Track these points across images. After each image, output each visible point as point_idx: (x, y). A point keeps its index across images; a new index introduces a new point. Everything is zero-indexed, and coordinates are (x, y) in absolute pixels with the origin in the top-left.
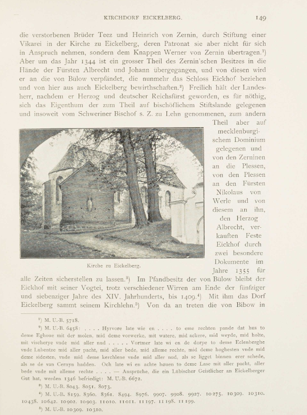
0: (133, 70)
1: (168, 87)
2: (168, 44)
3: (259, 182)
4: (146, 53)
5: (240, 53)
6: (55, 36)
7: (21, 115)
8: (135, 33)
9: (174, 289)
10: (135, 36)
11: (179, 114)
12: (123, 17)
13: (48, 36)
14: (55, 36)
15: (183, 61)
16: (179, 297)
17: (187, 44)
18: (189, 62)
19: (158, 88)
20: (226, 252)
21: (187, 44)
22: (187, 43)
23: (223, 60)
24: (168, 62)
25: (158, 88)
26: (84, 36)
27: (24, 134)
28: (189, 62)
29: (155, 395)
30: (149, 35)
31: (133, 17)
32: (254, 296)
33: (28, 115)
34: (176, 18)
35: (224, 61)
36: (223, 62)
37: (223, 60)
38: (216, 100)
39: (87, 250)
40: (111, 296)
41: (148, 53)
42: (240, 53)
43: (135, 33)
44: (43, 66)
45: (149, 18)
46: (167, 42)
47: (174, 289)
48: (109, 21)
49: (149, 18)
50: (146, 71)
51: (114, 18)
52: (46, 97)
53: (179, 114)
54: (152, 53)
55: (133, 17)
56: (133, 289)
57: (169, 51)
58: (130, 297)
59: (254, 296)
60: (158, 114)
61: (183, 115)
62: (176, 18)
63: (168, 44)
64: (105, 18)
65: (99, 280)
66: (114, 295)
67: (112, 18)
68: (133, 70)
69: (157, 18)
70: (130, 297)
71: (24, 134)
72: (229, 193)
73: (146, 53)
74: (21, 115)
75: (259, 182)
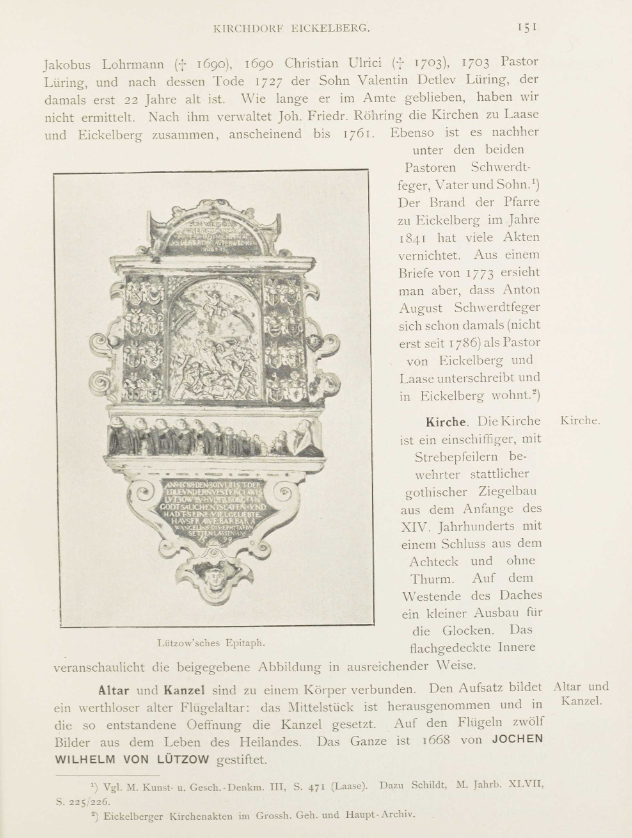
0: (288, 117)
8: (245, 739)
9: (254, 100)
10: (245, 744)
18: (92, 119)
19: (95, 669)
22: (112, 115)
28: (92, 119)
30: (306, 64)
31: (271, 29)
32: (404, 203)
36: (60, 744)
38: (459, 105)
40: (411, 527)
43: (245, 739)
44: (454, 142)
47: (254, 100)
50: (411, 546)
52: (146, 83)
55: (271, 29)
58: (157, 101)
59: (404, 203)
60: (403, 222)
64: (216, 29)
65: (491, 115)
66: (417, 525)
68: (288, 117)
70: (157, 101)
72: (66, 66)
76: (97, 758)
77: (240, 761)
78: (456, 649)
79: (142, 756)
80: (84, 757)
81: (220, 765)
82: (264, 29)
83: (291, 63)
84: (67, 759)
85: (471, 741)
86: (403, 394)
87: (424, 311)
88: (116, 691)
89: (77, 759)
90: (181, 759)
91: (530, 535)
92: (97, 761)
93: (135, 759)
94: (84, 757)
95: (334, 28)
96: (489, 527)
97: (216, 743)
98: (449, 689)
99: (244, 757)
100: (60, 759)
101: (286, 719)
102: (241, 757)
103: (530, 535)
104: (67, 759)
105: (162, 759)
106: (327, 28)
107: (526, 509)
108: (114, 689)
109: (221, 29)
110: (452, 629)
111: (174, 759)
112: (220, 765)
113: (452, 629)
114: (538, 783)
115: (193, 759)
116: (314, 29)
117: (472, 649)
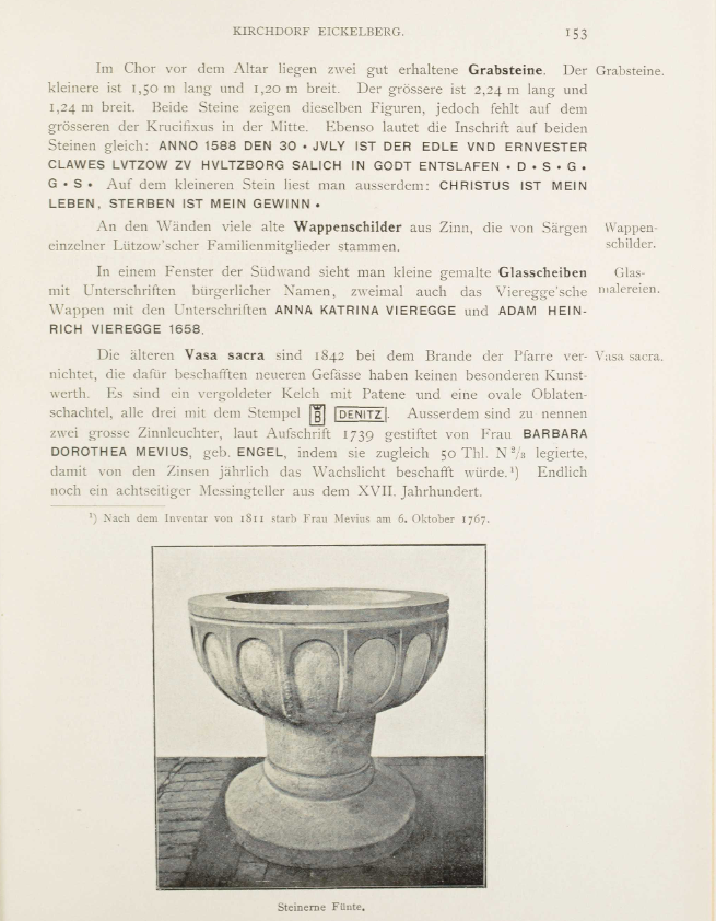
1: (428, 473)
2: (371, 395)
7: (650, 229)
12: (275, 30)
16: (526, 395)
17: (383, 71)
20: (371, 353)
21: (383, 71)
23: (431, 353)
24: (391, 357)
29: (417, 187)
31: (296, 31)
33: (240, 89)
34: (391, 32)
37: (431, 353)
45: (331, 31)
46: (367, 391)
48: (617, 352)
49: (331, 31)
51: (255, 32)
55: (296, 31)
59: (364, 88)
62: (391, 32)
63: (371, 395)
64: (236, 32)
67: (251, 31)
69: (349, 31)
74: (650, 229)
76: (274, 451)
77: (411, 435)
78: (313, 247)
80: (552, 308)
82: (289, 31)
83: (131, 68)
84: (394, 310)
86: (226, 124)
87: (374, 72)
89: (64, 164)
91: (574, 101)
92: (274, 453)
94: (552, 308)
95: (365, 31)
97: (466, 293)
98: (381, 274)
99: (416, 431)
100: (55, 491)
101: (151, 120)
102: (411, 431)
103: (574, 101)
104: (394, 310)
106: (358, 31)
109: (241, 31)
114: (657, 358)
116: (343, 32)
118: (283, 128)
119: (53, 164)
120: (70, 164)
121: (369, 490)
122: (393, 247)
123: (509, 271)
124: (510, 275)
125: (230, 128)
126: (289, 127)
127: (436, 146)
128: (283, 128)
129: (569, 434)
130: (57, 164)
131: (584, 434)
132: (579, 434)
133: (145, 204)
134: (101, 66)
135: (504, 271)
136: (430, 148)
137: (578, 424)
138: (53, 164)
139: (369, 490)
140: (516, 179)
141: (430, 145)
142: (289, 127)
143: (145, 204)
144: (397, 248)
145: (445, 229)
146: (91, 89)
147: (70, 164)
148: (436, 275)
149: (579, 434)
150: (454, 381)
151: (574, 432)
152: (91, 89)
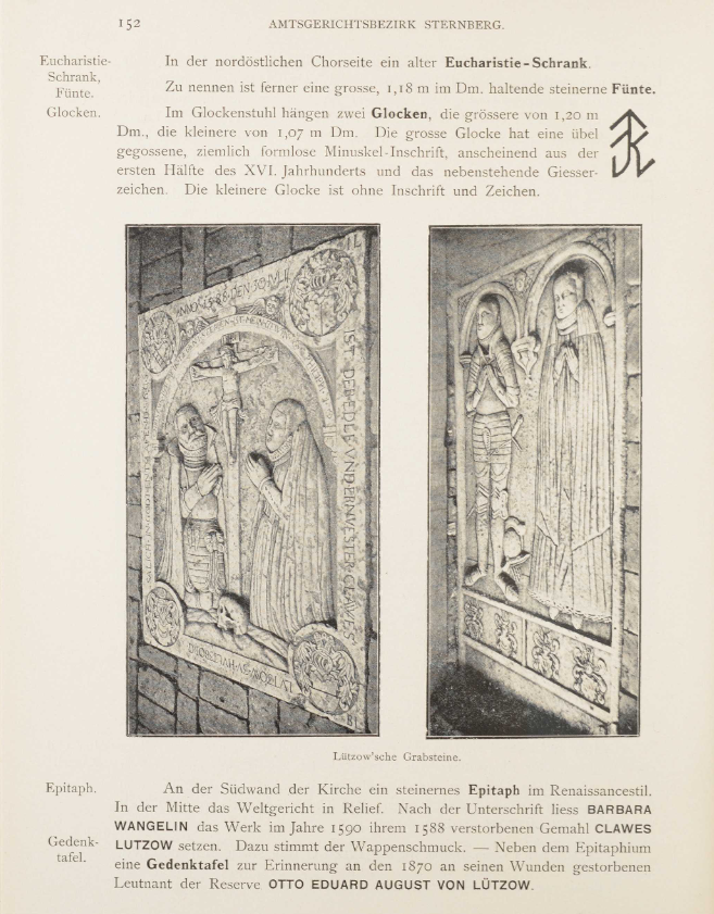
3: (491, 807)
4: (373, 848)
5: (354, 172)
6: (500, 830)
8: (170, 167)
11: (561, 868)
13: (486, 830)
14: (500, 830)
15: (493, 192)
18: (591, 90)
19: (513, 811)
25: (513, 811)
26: (260, 791)
27: (138, 236)
28: (591, 90)
31: (283, 24)
34: (491, 26)
35: (357, 846)
39: (244, 567)
41: (379, 848)
42: (354, 172)
48: (570, 70)
53: (561, 868)
54: (387, 848)
55: (283, 24)
56: (502, 811)
57: (248, 805)
61: (569, 870)
71: (138, 236)
73: (373, 848)
75: (491, 807)
79: (143, 829)
81: (338, 93)
85: (536, 116)
88: (496, 792)
89: (611, 828)
90: (499, 885)
92: (164, 827)
93: (450, 885)
94: (354, 887)
96: (545, 868)
99: (534, 807)
105: (479, 885)
107: (219, 172)
108: (493, 789)
110: (202, 110)
111: (135, 844)
112: (338, 93)
113: (202, 110)
115: (155, 845)
117: (222, 114)
118: (178, 809)
119: (600, 829)
120: (616, 829)
121: (255, 170)
122: (532, 192)
123: (382, 112)
124: (383, 115)
125: (174, 62)
126: (183, 808)
127: (325, 884)
128: (178, 809)
129: (633, 811)
130: (603, 829)
131: (648, 810)
132: (643, 811)
133: (615, 810)
134: (171, 110)
135: (377, 112)
136: (319, 886)
137: (643, 801)
138: (600, 829)
139: (255, 170)
140: (312, 798)
141: (320, 883)
142: (183, 808)
143: (615, 810)
144: (428, 116)
145: (171, 89)
146: (510, 116)
147: (616, 829)
148: (449, 192)
149: (643, 811)
150: (231, 93)
151: (638, 808)
152: (510, 116)
